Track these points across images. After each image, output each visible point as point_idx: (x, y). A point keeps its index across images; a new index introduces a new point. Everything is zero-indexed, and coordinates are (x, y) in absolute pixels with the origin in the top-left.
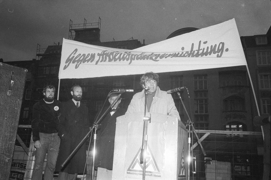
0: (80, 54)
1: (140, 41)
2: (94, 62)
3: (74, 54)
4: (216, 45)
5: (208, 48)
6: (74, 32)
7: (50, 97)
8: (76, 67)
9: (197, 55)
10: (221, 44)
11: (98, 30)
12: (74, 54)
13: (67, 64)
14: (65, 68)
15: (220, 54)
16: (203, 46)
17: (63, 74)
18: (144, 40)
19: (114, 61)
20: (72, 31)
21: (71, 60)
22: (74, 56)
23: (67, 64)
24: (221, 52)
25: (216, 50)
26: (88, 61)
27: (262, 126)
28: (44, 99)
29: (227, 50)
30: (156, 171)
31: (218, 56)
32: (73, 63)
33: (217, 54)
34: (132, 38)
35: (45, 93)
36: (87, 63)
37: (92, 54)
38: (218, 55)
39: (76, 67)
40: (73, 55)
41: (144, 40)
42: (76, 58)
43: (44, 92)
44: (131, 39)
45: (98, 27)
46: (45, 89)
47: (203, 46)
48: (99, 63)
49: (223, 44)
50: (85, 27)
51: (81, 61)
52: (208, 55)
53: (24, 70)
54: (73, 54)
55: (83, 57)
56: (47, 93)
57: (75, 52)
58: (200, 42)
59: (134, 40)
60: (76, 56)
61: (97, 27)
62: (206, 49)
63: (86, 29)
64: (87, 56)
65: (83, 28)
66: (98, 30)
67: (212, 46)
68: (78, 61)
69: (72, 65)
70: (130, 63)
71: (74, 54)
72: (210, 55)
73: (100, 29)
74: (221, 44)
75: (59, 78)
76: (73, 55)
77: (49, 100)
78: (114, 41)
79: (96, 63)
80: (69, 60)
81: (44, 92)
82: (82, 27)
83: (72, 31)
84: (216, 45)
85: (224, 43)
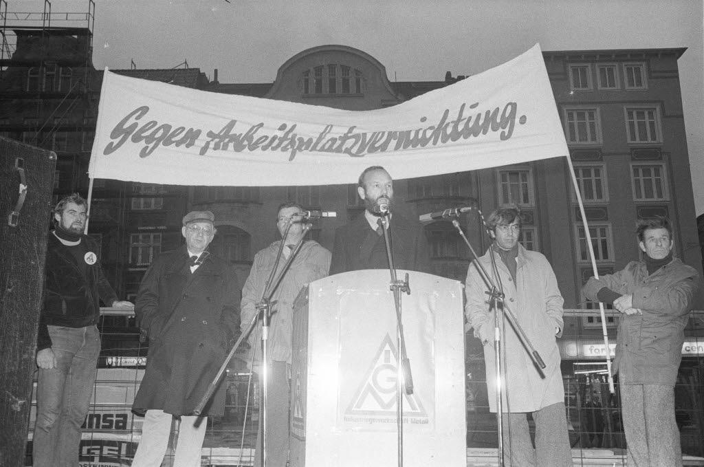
0: (155, 123)
1: (204, 73)
2: (195, 149)
3: (136, 119)
4: (498, 108)
5: (479, 115)
6: (14, 33)
7: (74, 226)
8: (144, 154)
9: (455, 136)
10: (510, 107)
11: (85, 34)
12: (137, 118)
13: (116, 141)
14: (109, 150)
15: (506, 130)
16: (467, 113)
17: (102, 167)
18: (216, 71)
19: (170, 127)
20: (7, 32)
21: (128, 132)
22: (136, 125)
23: (116, 141)
24: (509, 124)
25: (498, 121)
26: (178, 144)
27: (64, 312)
28: (54, 232)
29: (523, 120)
30: (417, 409)
31: (504, 137)
32: (136, 139)
33: (501, 130)
34: (186, 63)
35: (61, 216)
36: (176, 148)
37: (192, 129)
38: (503, 133)
39: (144, 154)
40: (132, 121)
41: (216, 71)
42: (143, 130)
43: (58, 211)
44: (183, 67)
45: (86, 26)
46: (61, 205)
47: (467, 113)
48: (210, 152)
49: (514, 106)
50: (47, 22)
51: (159, 140)
52: (481, 134)
53: (48, 155)
54: (135, 116)
55: (161, 131)
56: (66, 213)
57: (139, 112)
58: (464, 105)
59: (190, 69)
60: (142, 123)
61: (83, 25)
62: (474, 119)
63: (49, 27)
64: (175, 132)
65: (40, 24)
66: (85, 34)
67: (488, 112)
68: (149, 139)
69: (131, 149)
70: (291, 159)
71: (136, 119)
72: (485, 133)
73: (91, 30)
74: (510, 107)
75: (89, 177)
76: (132, 121)
77: (71, 235)
78: (133, 68)
79: (203, 151)
80: (120, 132)
81: (58, 211)
82: (36, 22)
83: (7, 32)
84: (498, 108)
85: (515, 104)
